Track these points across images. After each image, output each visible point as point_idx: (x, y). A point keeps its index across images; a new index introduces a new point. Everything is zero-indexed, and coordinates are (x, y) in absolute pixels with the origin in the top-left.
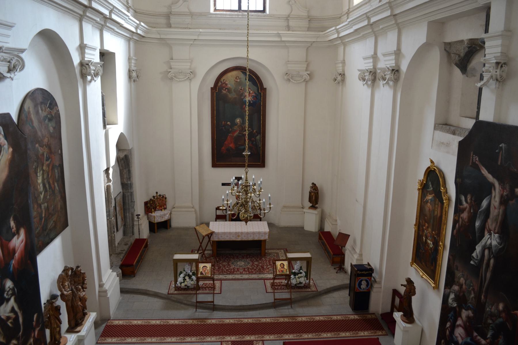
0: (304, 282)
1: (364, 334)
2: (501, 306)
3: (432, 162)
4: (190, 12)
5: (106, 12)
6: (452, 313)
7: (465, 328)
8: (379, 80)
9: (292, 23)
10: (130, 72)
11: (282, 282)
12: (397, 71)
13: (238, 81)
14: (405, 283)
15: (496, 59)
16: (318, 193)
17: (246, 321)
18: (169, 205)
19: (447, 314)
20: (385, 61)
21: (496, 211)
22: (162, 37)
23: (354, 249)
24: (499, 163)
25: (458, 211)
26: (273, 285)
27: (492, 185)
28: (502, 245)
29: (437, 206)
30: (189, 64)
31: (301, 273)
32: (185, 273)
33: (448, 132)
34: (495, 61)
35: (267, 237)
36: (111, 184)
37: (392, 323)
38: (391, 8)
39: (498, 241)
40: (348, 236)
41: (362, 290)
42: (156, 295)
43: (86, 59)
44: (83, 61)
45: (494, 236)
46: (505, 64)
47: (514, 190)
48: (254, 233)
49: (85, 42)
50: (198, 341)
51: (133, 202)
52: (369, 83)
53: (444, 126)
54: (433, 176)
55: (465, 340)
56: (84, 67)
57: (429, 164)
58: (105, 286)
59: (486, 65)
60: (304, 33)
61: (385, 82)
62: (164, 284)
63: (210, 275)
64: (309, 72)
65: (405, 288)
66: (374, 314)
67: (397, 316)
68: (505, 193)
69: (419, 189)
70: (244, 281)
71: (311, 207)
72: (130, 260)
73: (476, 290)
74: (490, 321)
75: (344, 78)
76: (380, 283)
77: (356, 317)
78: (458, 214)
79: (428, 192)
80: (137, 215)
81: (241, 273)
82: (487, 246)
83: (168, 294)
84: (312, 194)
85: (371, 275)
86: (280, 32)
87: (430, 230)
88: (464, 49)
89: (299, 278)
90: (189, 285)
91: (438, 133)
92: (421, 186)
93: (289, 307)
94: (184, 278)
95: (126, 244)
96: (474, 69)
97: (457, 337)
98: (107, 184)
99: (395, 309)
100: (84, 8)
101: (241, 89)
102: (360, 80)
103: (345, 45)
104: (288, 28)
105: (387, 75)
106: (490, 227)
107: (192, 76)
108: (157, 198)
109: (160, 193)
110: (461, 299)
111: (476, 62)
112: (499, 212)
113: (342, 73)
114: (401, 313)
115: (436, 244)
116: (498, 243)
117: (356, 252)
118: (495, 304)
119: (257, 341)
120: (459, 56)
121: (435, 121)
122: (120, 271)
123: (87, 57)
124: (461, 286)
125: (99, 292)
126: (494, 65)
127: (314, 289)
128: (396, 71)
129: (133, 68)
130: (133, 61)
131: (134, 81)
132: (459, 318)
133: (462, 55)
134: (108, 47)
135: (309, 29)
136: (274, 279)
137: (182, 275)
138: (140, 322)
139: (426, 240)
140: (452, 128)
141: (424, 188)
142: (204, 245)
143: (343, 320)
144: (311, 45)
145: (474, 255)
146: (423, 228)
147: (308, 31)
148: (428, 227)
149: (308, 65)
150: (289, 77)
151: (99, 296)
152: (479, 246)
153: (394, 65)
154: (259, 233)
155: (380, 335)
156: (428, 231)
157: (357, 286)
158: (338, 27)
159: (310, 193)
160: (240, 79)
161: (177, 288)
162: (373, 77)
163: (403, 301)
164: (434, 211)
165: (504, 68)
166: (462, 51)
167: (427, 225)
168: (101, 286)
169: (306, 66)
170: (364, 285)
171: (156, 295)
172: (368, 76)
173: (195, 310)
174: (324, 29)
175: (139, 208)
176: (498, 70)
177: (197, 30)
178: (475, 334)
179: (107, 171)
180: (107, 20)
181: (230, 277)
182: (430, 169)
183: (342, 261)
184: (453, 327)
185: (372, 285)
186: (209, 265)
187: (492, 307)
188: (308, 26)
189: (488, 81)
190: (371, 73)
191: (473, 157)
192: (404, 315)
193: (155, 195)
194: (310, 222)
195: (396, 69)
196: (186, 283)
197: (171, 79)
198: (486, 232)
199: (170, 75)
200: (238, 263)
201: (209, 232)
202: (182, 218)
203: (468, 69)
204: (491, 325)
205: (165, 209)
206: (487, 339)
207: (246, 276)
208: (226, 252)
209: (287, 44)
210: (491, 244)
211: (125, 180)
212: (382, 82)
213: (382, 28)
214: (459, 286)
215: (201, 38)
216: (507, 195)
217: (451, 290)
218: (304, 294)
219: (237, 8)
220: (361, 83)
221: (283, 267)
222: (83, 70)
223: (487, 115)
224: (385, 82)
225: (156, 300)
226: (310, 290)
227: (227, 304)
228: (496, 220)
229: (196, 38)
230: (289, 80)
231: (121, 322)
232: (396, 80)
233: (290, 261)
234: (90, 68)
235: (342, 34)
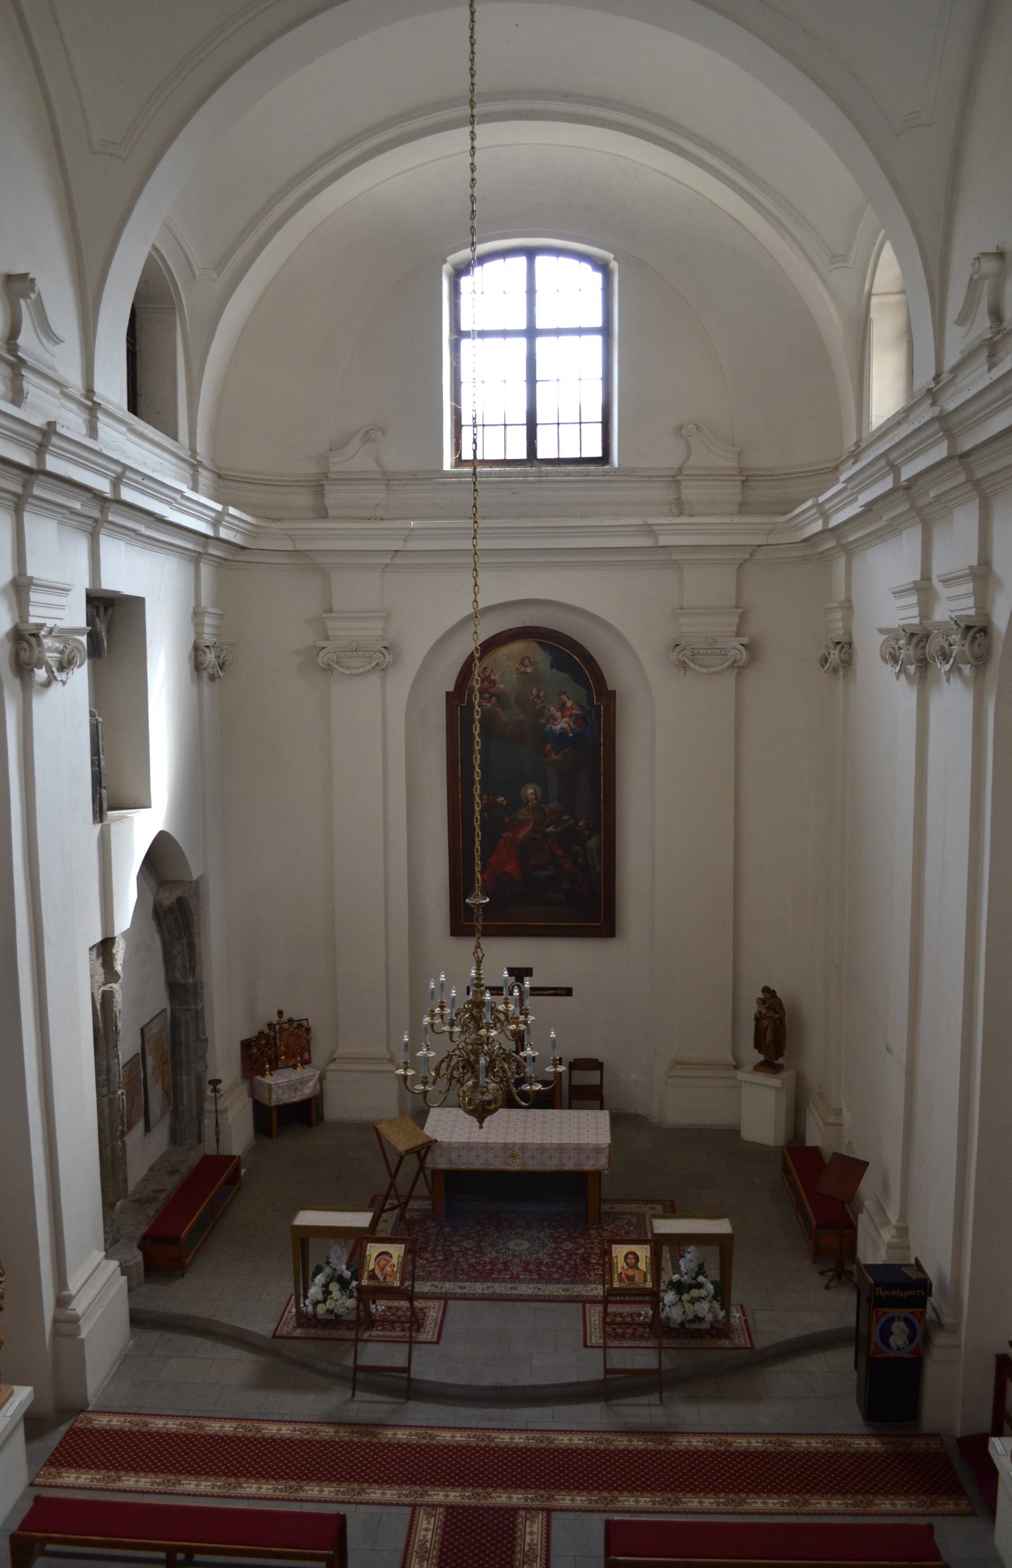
0: (709, 1317)
1: (892, 1508)
4: (384, 473)
5: (103, 485)
9: (688, 493)
10: (197, 651)
11: (639, 1315)
13: (529, 670)
16: (782, 1020)
17: (505, 1438)
18: (319, 1051)
22: (301, 546)
26: (607, 1321)
30: (381, 624)
31: (700, 1286)
32: (328, 1270)
35: (603, 1162)
36: (116, 986)
38: (949, 434)
40: (866, 1164)
41: (891, 1354)
42: (238, 1339)
43: (32, 620)
44: (22, 627)
48: (561, 1148)
49: (30, 573)
50: (340, 1497)
51: (202, 1041)
52: (912, 669)
56: (25, 645)
58: (74, 1304)
60: (727, 520)
62: (261, 1301)
63: (397, 1284)
64: (745, 640)
66: (936, 1436)
70: (518, 1304)
71: (761, 1064)
72: (170, 1226)
75: (851, 656)
76: (955, 1330)
77: (875, 1444)
80: (210, 1082)
81: (514, 1278)
83: (274, 1336)
84: (765, 1023)
86: (650, 521)
89: (692, 1302)
90: (341, 1311)
93: (654, 1398)
94: (326, 1286)
95: (172, 1172)
98: (106, 988)
100: (26, 476)
101: (538, 696)
102: (885, 660)
103: (849, 552)
104: (679, 506)
105: (955, 643)
107: (389, 658)
108: (282, 1029)
109: (292, 1012)
113: (843, 639)
117: (887, 1222)
119: (528, 1509)
122: (139, 1257)
123: (36, 615)
125: (56, 1321)
127: (741, 1341)
129: (208, 639)
130: (207, 620)
131: (212, 678)
134: (110, 583)
135: (744, 507)
136: (605, 1301)
137: (320, 1279)
138: (172, 1425)
142: (403, 1182)
143: (826, 1453)
144: (752, 554)
147: (740, 513)
149: (742, 617)
150: (684, 656)
151: (56, 1334)
153: (972, 612)
154: (579, 1148)
157: (876, 1338)
158: (821, 499)
159: (757, 1019)
160: (534, 664)
161: (305, 1320)
162: (919, 652)
168: (62, 1302)
169: (736, 620)
170: (899, 1337)
171: (238, 1339)
172: (907, 652)
173: (350, 1392)
174: (784, 506)
175: (223, 1060)
177: (400, 524)
179: (105, 947)
180: (107, 505)
181: (478, 1288)
185: (927, 1340)
186: (397, 1251)
188: (739, 498)
190: (915, 640)
193: (275, 1019)
194: (759, 1113)
195: (979, 623)
196: (330, 1304)
197: (328, 669)
199: (322, 658)
200: (511, 1245)
201: (420, 1142)
202: (358, 1093)
205: (306, 1062)
207: (526, 1289)
208: (469, 1208)
209: (675, 557)
211: (178, 973)
213: (937, 498)
215: (412, 545)
218: (707, 1356)
219: (523, 455)
220: (890, 670)
221: (635, 1266)
222: (22, 653)
225: (236, 1353)
226: (727, 1343)
227: (452, 1380)
229: (399, 545)
230: (683, 665)
231: (116, 1422)
232: (981, 660)
233: (658, 1243)
234: (40, 644)
235: (835, 521)
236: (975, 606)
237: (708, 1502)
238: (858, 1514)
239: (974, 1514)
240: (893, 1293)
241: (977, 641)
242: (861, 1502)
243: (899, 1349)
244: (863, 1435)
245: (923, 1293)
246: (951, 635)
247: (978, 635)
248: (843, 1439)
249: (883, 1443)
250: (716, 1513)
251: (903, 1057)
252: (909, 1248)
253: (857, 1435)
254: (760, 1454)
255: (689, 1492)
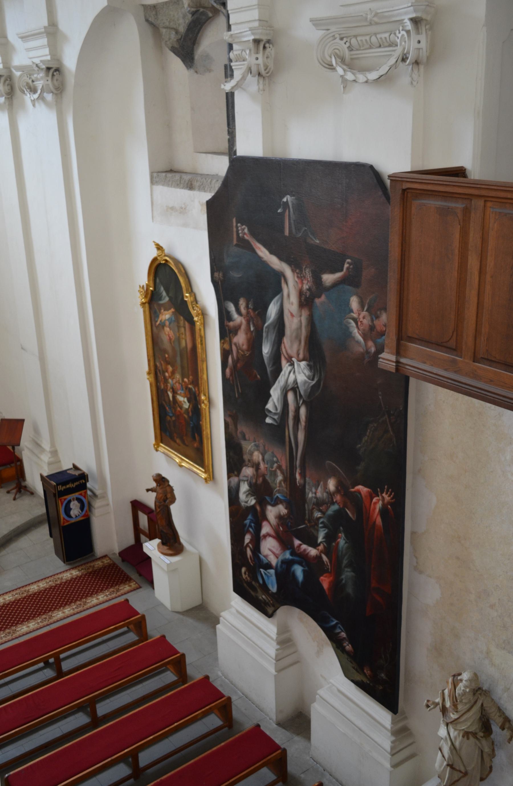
1: (99, 601)
2: (332, 485)
3: (159, 248)
6: (250, 517)
7: (278, 537)
8: (23, 92)
12: (57, 70)
14: (154, 485)
15: (253, 34)
19: (243, 521)
20: (28, 50)
21: (296, 320)
23: (38, 445)
24: (287, 233)
25: (226, 332)
27: (279, 276)
28: (316, 380)
29: (182, 330)
33: (178, 185)
34: (252, 38)
37: (146, 561)
39: (307, 372)
40: (21, 422)
41: (73, 521)
45: (299, 365)
46: (269, 41)
47: (320, 279)
53: (169, 175)
54: (166, 276)
55: (281, 558)
57: (154, 253)
59: (235, 47)
61: (36, 96)
65: (154, 494)
66: (106, 556)
67: (151, 547)
68: (306, 287)
69: (143, 304)
73: (284, 467)
74: (317, 514)
76: (104, 496)
77: (75, 573)
78: (227, 339)
79: (160, 306)
82: (290, 387)
85: (83, 487)
87: (178, 376)
88: (184, 17)
91: (160, 190)
92: (146, 297)
96: (207, 57)
97: (266, 556)
99: (143, 537)
106: (289, 352)
110: (262, 491)
111: (211, 40)
112: (301, 321)
114: (157, 541)
115: (194, 399)
116: (309, 378)
117: (43, 450)
118: (322, 483)
120: (177, 32)
121: (151, 166)
124: (257, 466)
126: (251, 45)
128: (54, 70)
132: (265, 523)
133: (182, 29)
139: (174, 397)
140: (186, 177)
141: (151, 301)
143: (51, 587)
145: (269, 406)
146: (165, 377)
148: (173, 373)
152: (275, 389)
153: (49, 58)
155: (128, 592)
156: (176, 380)
157: (63, 515)
163: (157, 520)
164: (179, 340)
165: (268, 50)
166: (181, 21)
167: (170, 369)
176: (260, 56)
178: (297, 542)
182: (157, 263)
183: (21, 474)
184: (257, 540)
187: (316, 489)
189: (243, 78)
191: (237, 227)
192: (163, 543)
195: (54, 66)
198: (284, 362)
203: (196, 57)
204: (321, 520)
206: (319, 545)
210: (295, 382)
212: (28, 98)
214: (253, 467)
216: (309, 289)
217: (241, 477)
223: (250, 144)
224: (36, 96)
228: (298, 337)
232: (59, 90)
236: (50, 54)
237: (32, 625)
238: (81, 612)
239: (140, 587)
240: (68, 486)
241: (55, 78)
242: (80, 604)
243: (76, 516)
244: (67, 571)
245: (84, 481)
246: (33, 75)
247: (55, 73)
248: (56, 577)
249: (79, 570)
250: (107, 601)
251: (35, 350)
252: (60, 461)
253: (64, 572)
254: (14, 602)
255: (54, 610)
